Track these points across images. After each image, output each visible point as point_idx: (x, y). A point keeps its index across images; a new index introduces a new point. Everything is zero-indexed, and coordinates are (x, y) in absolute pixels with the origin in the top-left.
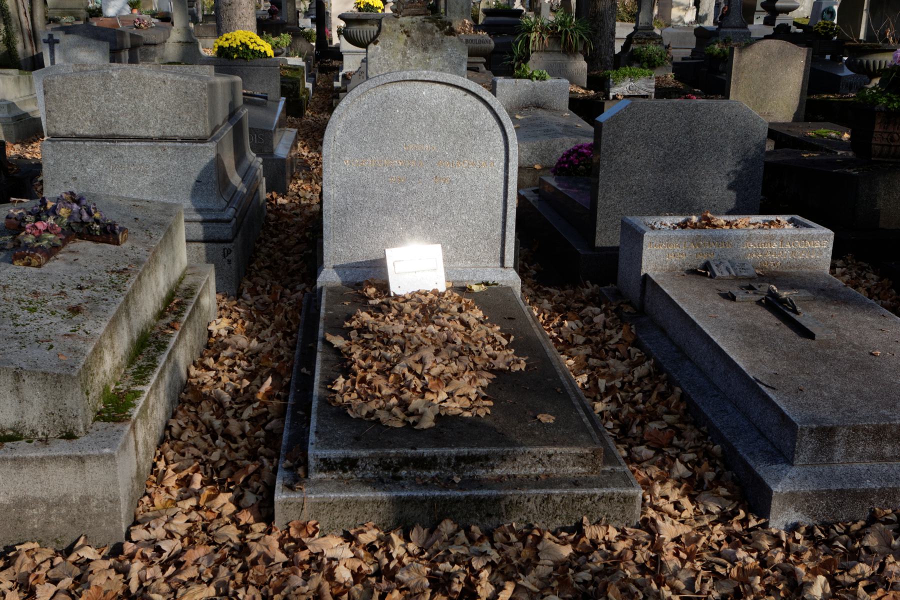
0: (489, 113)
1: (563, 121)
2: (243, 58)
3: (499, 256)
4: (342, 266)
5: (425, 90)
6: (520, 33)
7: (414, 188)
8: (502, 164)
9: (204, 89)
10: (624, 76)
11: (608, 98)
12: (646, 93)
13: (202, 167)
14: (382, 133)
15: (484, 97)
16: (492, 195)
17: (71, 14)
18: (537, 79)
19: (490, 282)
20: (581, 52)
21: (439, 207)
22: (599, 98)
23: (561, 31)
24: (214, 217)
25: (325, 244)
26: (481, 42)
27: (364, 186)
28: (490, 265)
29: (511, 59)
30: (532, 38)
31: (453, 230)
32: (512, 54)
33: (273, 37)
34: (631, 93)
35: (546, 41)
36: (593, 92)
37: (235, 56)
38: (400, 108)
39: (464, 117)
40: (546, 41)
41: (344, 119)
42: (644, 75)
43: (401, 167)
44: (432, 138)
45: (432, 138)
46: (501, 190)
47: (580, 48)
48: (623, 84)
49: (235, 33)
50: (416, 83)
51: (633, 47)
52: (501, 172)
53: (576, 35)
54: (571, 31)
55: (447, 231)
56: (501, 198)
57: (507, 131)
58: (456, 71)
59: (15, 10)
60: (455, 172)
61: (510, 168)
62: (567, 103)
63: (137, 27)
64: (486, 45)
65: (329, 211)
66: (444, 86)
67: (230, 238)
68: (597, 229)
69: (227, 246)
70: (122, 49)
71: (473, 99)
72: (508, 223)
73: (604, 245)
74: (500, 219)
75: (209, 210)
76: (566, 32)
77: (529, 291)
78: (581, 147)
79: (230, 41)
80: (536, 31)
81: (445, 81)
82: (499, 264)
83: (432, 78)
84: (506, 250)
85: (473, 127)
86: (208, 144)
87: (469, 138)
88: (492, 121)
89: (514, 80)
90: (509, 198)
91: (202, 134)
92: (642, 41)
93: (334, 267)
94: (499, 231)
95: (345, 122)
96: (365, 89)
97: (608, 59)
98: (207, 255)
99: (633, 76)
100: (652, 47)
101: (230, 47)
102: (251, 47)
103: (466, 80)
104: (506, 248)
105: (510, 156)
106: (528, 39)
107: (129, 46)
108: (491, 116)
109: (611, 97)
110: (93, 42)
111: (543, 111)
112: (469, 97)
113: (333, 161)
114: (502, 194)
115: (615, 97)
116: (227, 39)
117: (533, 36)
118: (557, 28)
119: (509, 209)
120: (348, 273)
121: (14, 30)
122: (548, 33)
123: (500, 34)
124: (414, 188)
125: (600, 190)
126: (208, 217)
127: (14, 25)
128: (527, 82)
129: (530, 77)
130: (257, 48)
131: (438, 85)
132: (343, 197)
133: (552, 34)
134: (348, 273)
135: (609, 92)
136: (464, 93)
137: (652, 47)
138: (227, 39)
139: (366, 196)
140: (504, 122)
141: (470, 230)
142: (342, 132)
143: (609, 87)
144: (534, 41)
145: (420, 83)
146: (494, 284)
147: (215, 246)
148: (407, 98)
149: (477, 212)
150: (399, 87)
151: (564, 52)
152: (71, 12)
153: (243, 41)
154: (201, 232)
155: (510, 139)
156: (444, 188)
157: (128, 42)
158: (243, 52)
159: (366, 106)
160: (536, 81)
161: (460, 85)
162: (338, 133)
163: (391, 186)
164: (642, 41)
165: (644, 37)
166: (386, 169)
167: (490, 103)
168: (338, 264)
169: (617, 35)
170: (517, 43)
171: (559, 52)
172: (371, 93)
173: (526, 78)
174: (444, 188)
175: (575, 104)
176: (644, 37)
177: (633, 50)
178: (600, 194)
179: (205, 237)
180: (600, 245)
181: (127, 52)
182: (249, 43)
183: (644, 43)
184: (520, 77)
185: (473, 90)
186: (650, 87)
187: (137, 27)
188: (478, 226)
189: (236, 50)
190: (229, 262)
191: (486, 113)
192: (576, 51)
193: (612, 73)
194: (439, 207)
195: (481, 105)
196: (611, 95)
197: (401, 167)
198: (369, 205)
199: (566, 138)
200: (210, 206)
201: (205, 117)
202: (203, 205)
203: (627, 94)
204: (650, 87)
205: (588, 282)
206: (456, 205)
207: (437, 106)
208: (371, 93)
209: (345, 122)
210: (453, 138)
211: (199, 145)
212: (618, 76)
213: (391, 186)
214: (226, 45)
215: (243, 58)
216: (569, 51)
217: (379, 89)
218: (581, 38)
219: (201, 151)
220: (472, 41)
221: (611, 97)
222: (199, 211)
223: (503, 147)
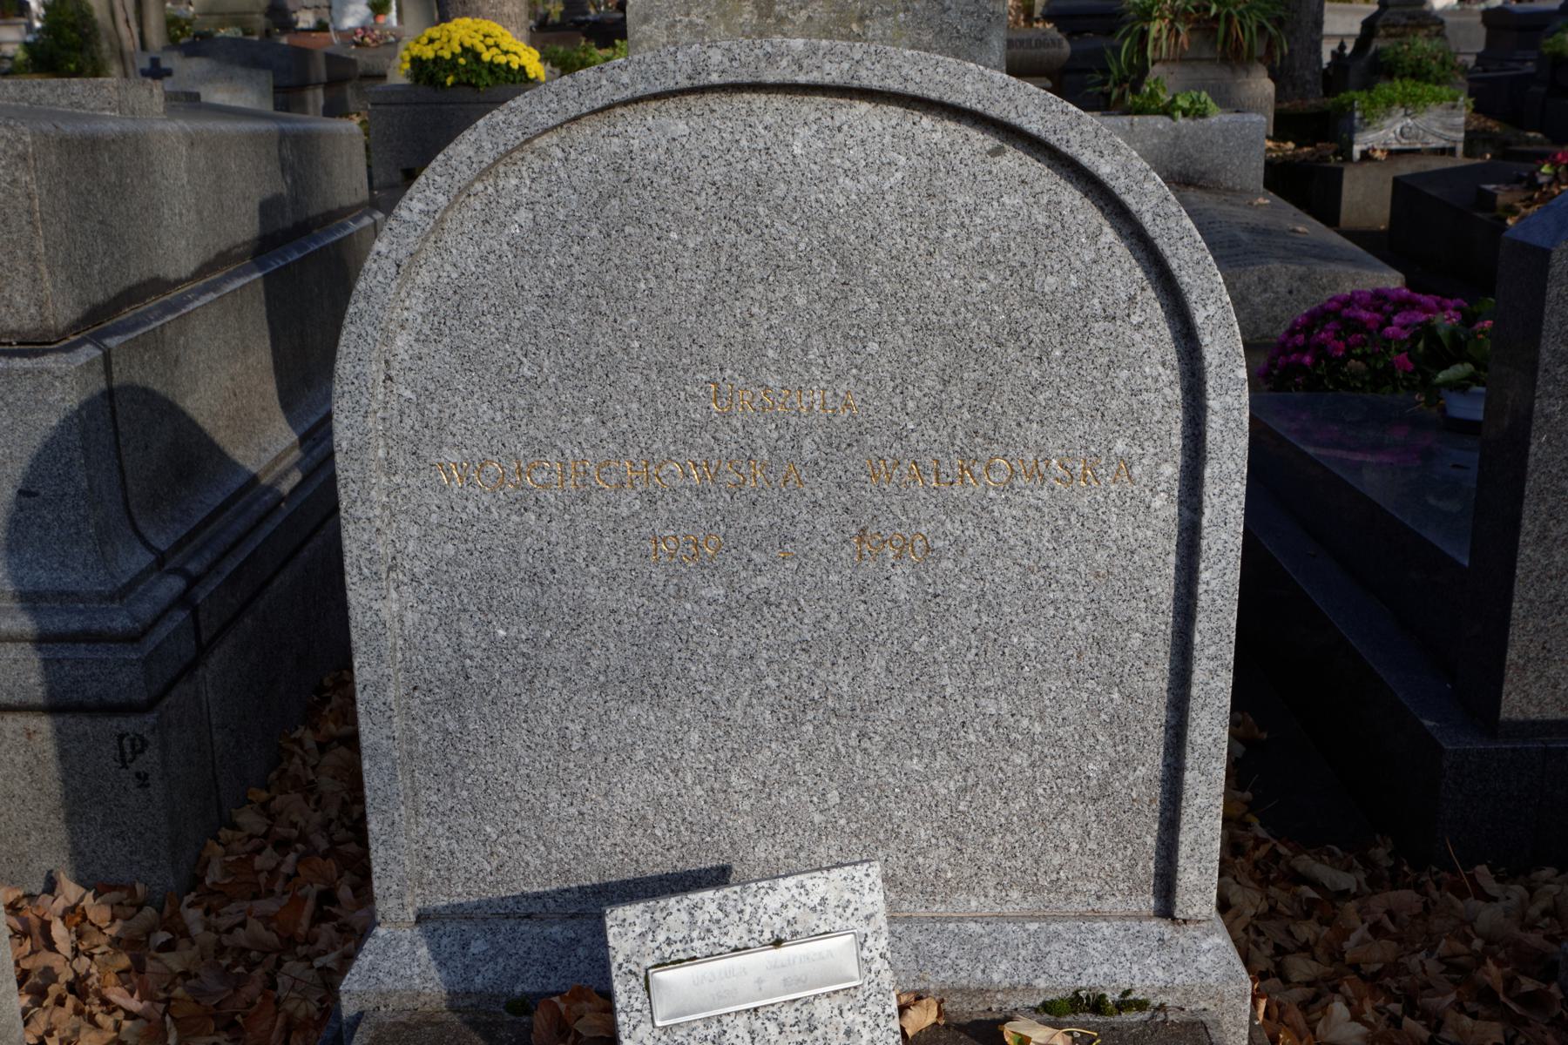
0: (1109, 235)
1: (1251, 217)
2: (469, 84)
3: (1147, 867)
4: (459, 913)
5: (804, 130)
6: (1125, 23)
7: (763, 581)
8: (1170, 471)
9: (23, 157)
10: (1390, 103)
11: (1348, 157)
12: (1441, 143)
13: (37, 441)
14: (604, 338)
15: (1087, 158)
16: (1121, 610)
17: (236, 23)
18: (1185, 114)
19: (1112, 996)
20: (1260, 60)
21: (877, 663)
22: (1325, 159)
23: (1217, 16)
24: (75, 624)
25: (373, 826)
26: (1041, 43)
27: (533, 578)
28: (1107, 905)
29: (1105, 83)
30: (1153, 33)
31: (942, 759)
32: (1106, 71)
33: (600, 47)
34: (1405, 144)
35: (1183, 38)
36: (1291, 145)
37: (450, 80)
38: (683, 222)
39: (987, 257)
40: (1183, 38)
41: (424, 277)
42: (1438, 99)
43: (700, 493)
44: (840, 359)
45: (840, 359)
46: (1164, 587)
47: (1260, 48)
48: (1387, 122)
49: (450, 26)
50: (759, 100)
51: (1377, 44)
52: (1165, 507)
53: (1252, 23)
54: (1240, 13)
55: (915, 764)
56: (1164, 623)
57: (1199, 317)
58: (963, 45)
59: (107, 15)
60: (952, 508)
61: (1210, 489)
62: (1261, 173)
63: (357, 44)
64: (1053, 51)
65: (379, 687)
66: (895, 112)
67: (140, 697)
68: (1512, 655)
69: (130, 724)
70: (304, 85)
71: (1035, 168)
72: (1194, 735)
73: (1534, 713)
74: (1157, 716)
75: (64, 596)
76: (1229, 17)
77: (1250, 901)
78: (1349, 301)
79: (437, 45)
80: (1162, 18)
81: (894, 84)
82: (1148, 902)
83: (833, 73)
84: (1184, 850)
85: (1036, 300)
86: (49, 361)
87: (1012, 351)
88: (1128, 273)
89: (1126, 120)
90: (1202, 624)
91: (28, 325)
92: (1399, 30)
93: (422, 918)
94: (1152, 763)
95: (432, 292)
96: (513, 135)
97: (1309, 77)
98: (63, 755)
99: (1411, 104)
100: (1422, 43)
101: (438, 60)
102: (486, 57)
103: (1000, 77)
104: (1186, 838)
105: (1212, 436)
106: (1144, 34)
107: (323, 77)
108: (1121, 249)
109: (1356, 154)
110: (239, 71)
111: (1199, 193)
112: (1014, 161)
113: (390, 468)
114: (1168, 604)
115: (1366, 156)
116: (431, 41)
117: (1154, 28)
118: (1208, 9)
119: (1199, 675)
120: (477, 947)
121: (106, 54)
122: (1187, 21)
123: (1079, 33)
124: (763, 581)
125: (1527, 511)
126: (57, 623)
127: (105, 46)
128: (1160, 122)
129: (1167, 111)
130: (502, 59)
131: (863, 107)
132: (444, 623)
133: (1197, 21)
134: (477, 947)
135: (1351, 143)
136: (991, 142)
137: (1422, 43)
138: (431, 41)
139: (544, 621)
140: (1185, 278)
141: (1020, 759)
142: (421, 339)
143: (1352, 131)
144: (1156, 40)
145: (779, 101)
146: (1126, 1003)
147: (85, 724)
148: (718, 173)
149: (1053, 684)
150: (675, 123)
151: (1225, 60)
152: (237, 18)
153: (467, 44)
154: (35, 679)
155: (1211, 356)
156: (901, 583)
157: (320, 71)
158: (467, 70)
159: (523, 215)
160: (1181, 121)
161: (971, 103)
162: (401, 341)
163: (659, 577)
164: (1399, 30)
165: (1404, 21)
166: (629, 502)
167: (1119, 186)
168: (442, 901)
169: (1327, 29)
170: (1117, 50)
171: (1212, 60)
172: (543, 154)
173: (1156, 113)
174: (901, 583)
175: (1280, 177)
176: (1404, 21)
177: (1378, 52)
178: (1526, 524)
179: (51, 692)
180: (1516, 715)
181: (320, 92)
182: (480, 47)
183: (1402, 35)
184: (1141, 111)
185: (1034, 128)
186: (1453, 128)
187: (357, 44)
188: (1058, 742)
189: (452, 65)
190: (142, 779)
191: (1094, 237)
192: (1250, 57)
193: (1359, 99)
194: (877, 663)
195: (1071, 196)
196: (1357, 149)
197: (700, 493)
198: (561, 657)
199: (1275, 265)
200: (71, 580)
201: (33, 259)
202: (44, 578)
203: (1395, 146)
204: (1453, 128)
205: (1482, 870)
206: (953, 655)
207: (860, 206)
208: (543, 154)
209: (432, 292)
210: (937, 356)
211: (18, 363)
212: (1373, 103)
213: (659, 577)
214: (429, 53)
215: (469, 84)
216: (1235, 57)
217: (582, 133)
218: (1262, 28)
219: (28, 384)
220: (1022, 42)
221: (1356, 154)
222: (30, 599)
223: (1176, 394)
